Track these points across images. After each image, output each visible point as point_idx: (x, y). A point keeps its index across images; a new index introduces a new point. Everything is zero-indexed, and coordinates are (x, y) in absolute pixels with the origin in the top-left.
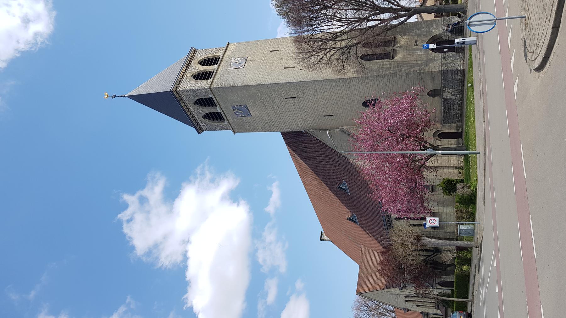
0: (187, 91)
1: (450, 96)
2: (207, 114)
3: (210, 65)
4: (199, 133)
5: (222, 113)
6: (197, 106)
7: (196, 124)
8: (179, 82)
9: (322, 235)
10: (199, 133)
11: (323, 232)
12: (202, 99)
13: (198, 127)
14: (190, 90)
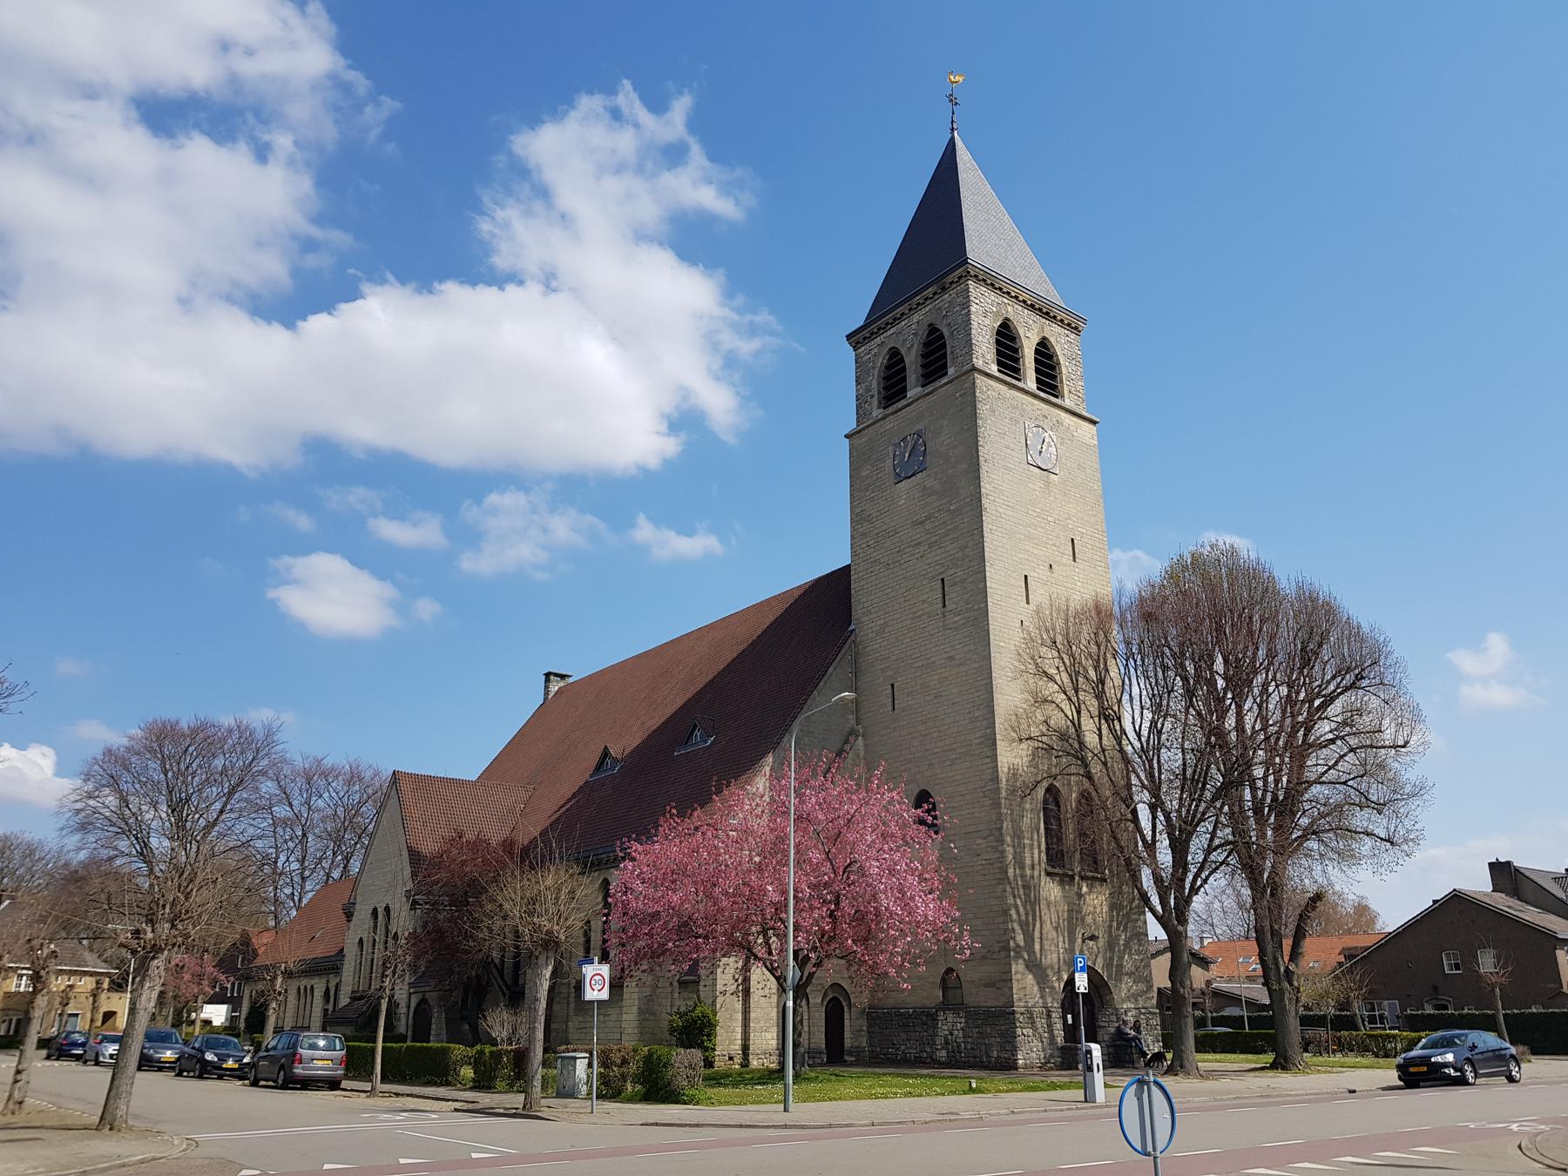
0: (966, 305)
1: (943, 1029)
2: (902, 360)
3: (1037, 371)
4: (849, 337)
5: (903, 402)
6: (923, 332)
7: (874, 328)
8: (992, 282)
9: (563, 677)
10: (849, 337)
11: (571, 680)
12: (944, 346)
13: (866, 333)
14: (969, 314)
